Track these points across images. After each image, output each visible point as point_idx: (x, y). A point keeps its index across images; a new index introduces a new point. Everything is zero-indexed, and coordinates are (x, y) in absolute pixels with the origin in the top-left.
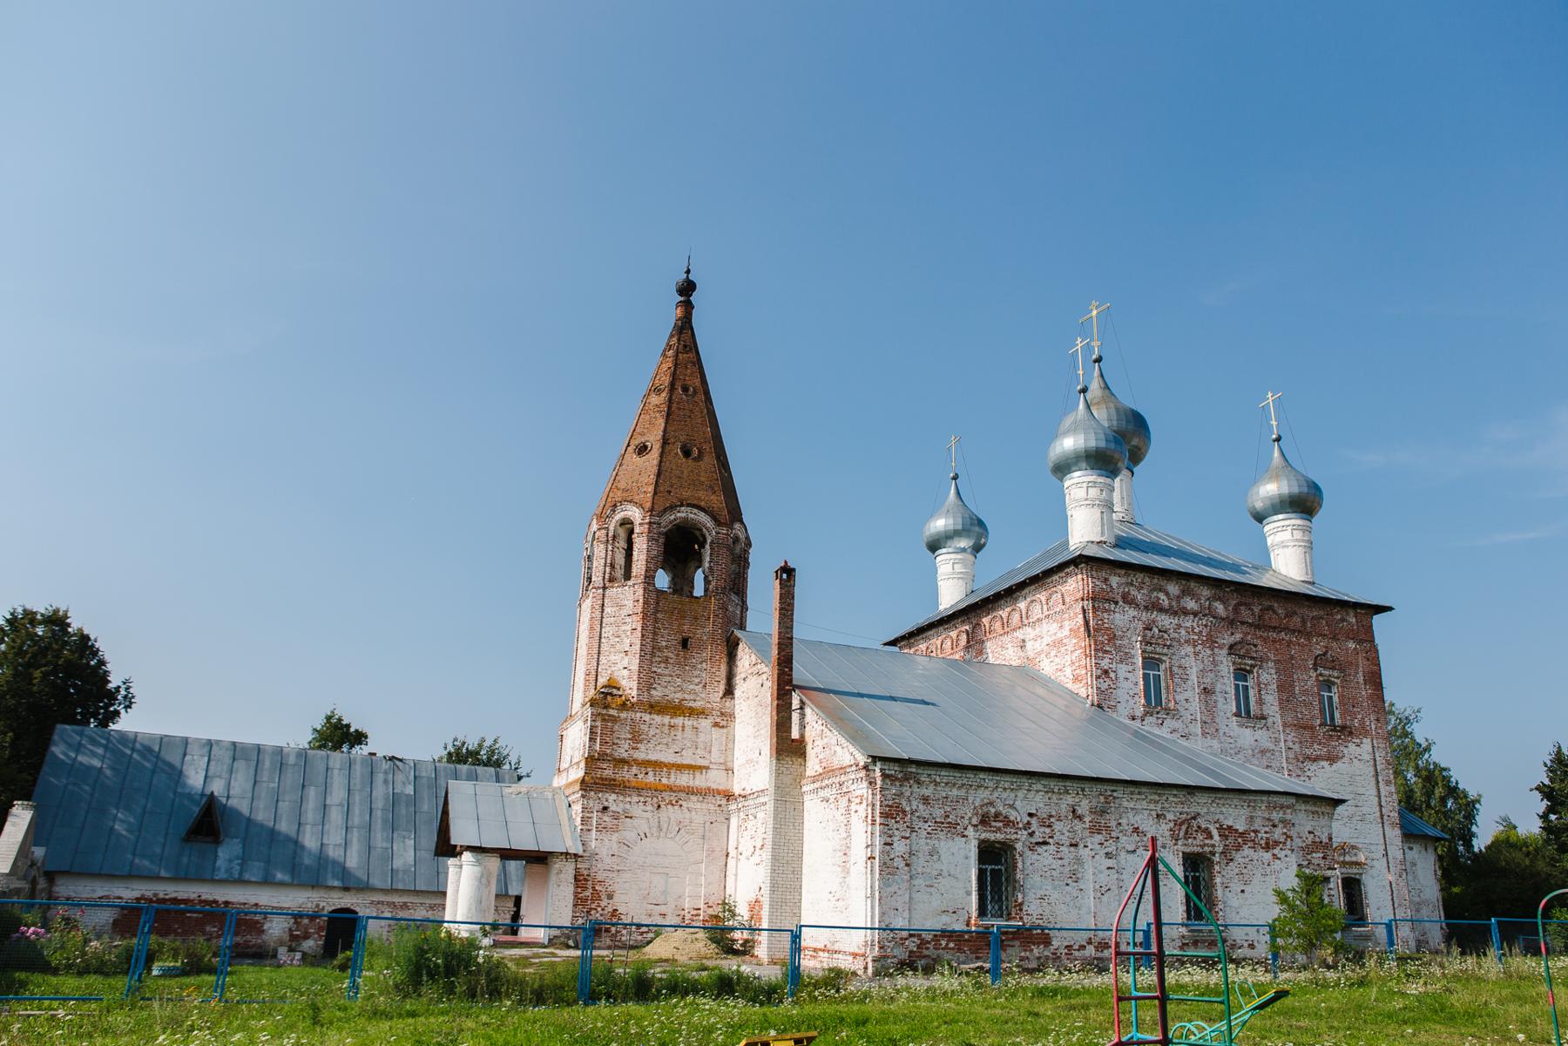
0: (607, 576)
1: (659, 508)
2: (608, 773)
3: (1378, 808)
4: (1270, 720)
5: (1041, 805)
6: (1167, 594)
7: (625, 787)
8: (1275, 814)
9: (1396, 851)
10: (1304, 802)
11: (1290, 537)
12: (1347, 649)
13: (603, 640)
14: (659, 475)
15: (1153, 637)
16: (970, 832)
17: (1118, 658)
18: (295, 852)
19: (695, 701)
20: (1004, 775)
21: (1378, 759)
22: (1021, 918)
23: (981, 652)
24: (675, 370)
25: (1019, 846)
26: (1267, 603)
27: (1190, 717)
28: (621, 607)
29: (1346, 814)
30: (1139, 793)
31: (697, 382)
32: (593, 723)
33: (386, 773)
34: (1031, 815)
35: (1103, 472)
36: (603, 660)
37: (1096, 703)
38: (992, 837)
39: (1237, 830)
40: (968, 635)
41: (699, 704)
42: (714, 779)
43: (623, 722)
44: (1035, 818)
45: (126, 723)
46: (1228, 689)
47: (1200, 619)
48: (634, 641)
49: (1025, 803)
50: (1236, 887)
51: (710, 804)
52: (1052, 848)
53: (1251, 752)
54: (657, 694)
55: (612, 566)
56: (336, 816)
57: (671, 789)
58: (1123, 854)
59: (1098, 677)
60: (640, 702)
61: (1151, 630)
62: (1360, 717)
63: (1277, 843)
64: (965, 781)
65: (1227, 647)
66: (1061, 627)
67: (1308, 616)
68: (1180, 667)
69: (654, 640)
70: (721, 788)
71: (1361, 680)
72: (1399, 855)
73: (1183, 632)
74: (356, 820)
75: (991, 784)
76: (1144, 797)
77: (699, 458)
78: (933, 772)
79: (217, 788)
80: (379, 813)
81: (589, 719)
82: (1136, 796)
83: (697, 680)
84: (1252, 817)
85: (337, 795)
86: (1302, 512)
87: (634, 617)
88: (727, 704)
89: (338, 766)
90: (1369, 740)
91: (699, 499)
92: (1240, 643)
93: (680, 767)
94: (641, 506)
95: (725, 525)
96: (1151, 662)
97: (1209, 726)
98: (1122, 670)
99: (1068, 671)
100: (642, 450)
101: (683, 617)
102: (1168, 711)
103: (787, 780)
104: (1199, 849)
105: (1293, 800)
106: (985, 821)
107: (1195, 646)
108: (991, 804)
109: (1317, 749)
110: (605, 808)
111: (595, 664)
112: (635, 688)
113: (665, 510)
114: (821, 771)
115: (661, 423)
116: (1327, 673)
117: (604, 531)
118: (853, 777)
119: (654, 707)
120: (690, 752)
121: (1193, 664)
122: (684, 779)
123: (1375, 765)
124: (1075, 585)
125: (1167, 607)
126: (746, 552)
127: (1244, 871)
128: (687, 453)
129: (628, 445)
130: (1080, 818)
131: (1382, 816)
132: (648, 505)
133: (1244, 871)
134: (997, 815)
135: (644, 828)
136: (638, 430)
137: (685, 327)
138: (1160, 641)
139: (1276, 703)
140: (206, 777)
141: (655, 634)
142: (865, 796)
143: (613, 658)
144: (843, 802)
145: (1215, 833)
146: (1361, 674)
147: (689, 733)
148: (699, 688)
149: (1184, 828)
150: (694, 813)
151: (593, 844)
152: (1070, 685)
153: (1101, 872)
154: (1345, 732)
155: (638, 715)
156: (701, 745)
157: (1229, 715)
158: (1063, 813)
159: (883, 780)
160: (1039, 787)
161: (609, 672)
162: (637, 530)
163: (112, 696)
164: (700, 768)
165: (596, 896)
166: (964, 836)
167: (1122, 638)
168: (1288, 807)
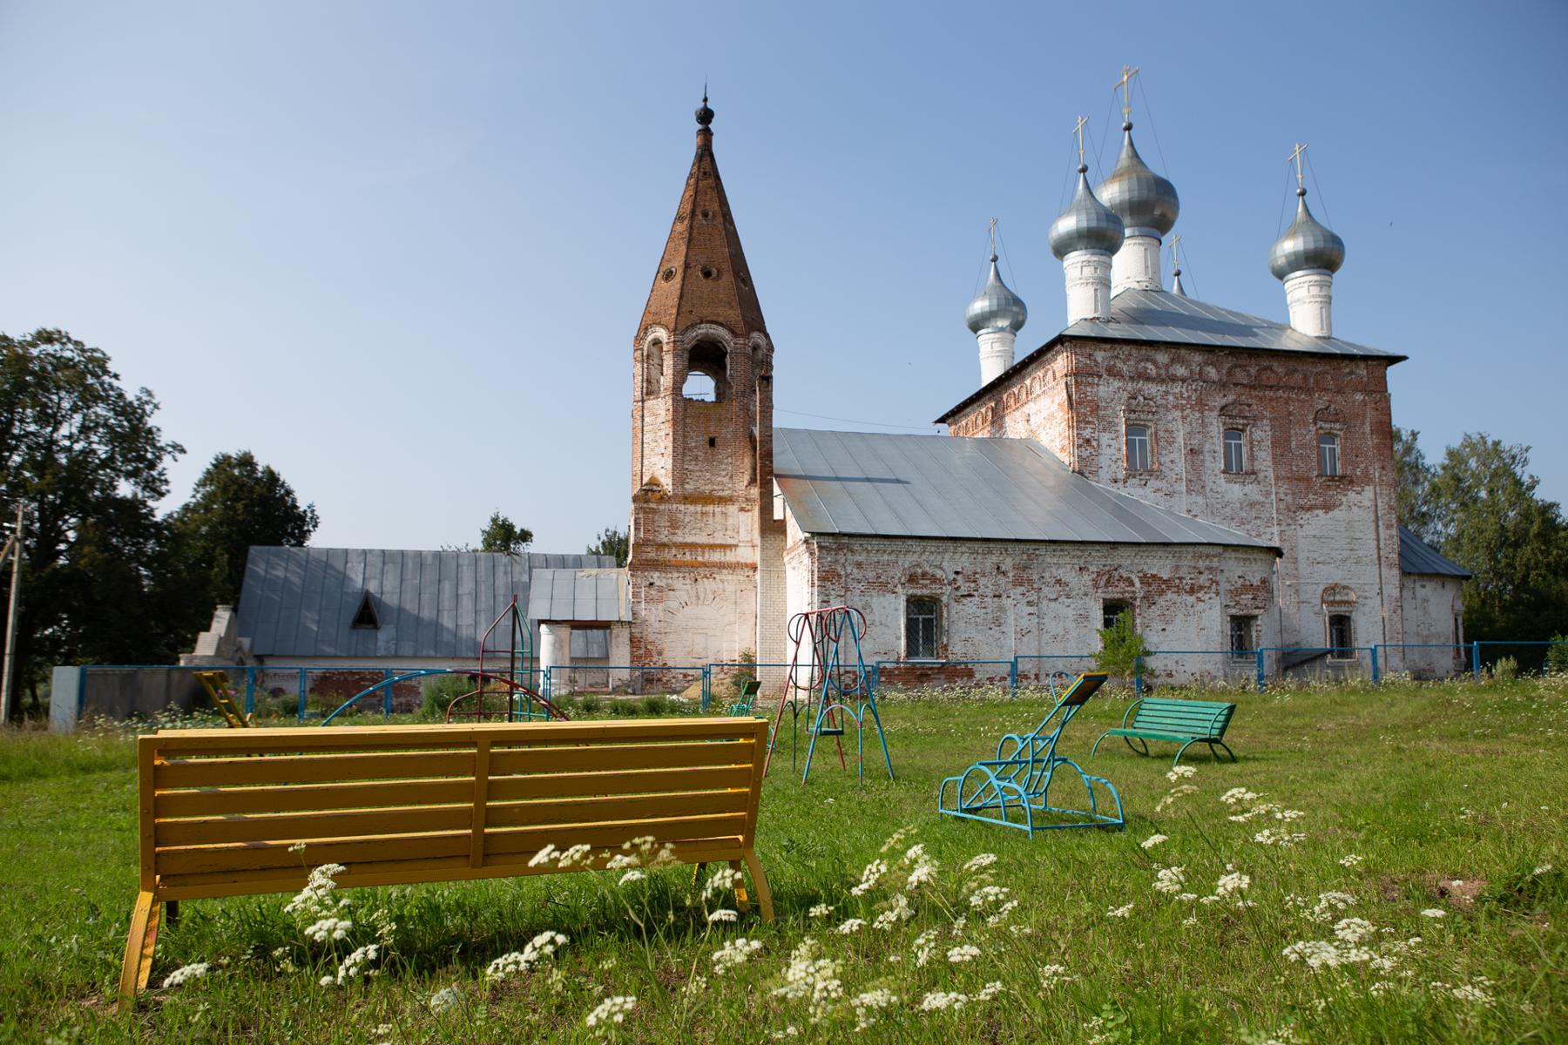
0: (645, 390)
1: (681, 327)
2: (652, 555)
3: (1376, 551)
4: (1261, 475)
5: (967, 564)
6: (1155, 363)
7: (666, 566)
8: (1201, 562)
9: (1392, 590)
10: (1234, 550)
11: (1307, 294)
12: (1354, 402)
14: (681, 297)
15: (1138, 405)
16: (899, 589)
17: (1101, 427)
18: (436, 632)
21: (1379, 504)
22: (946, 657)
23: (1001, 427)
24: (695, 198)
25: (944, 599)
26: (1267, 363)
27: (1175, 477)
28: (656, 416)
29: (1340, 557)
30: (1061, 550)
31: (716, 206)
33: (505, 565)
35: (1097, 251)
37: (1077, 469)
38: (919, 592)
41: (727, 492)
43: (662, 513)
44: (960, 576)
45: (317, 540)
46: (1217, 448)
49: (950, 563)
51: (740, 576)
52: (976, 599)
53: (1238, 505)
54: (690, 487)
56: (466, 603)
57: (704, 565)
58: (1045, 602)
59: (1079, 446)
60: (675, 495)
62: (1363, 466)
63: (1201, 588)
64: (894, 548)
65: (1218, 409)
67: (1312, 372)
68: (1166, 431)
69: (684, 442)
70: (749, 561)
71: (1367, 429)
72: (1396, 592)
73: (1171, 398)
74: (483, 605)
75: (918, 549)
77: (719, 276)
79: (373, 587)
80: (502, 599)
82: (1058, 553)
83: (724, 473)
84: (1177, 566)
85: (467, 586)
86: (1319, 267)
89: (466, 562)
90: (1371, 487)
91: (718, 315)
92: (1233, 404)
93: (713, 547)
94: (666, 327)
95: (742, 336)
96: (1134, 428)
97: (1196, 484)
100: (668, 275)
101: (709, 420)
102: (1151, 473)
103: (771, 553)
104: (1120, 596)
105: (1221, 550)
106: (912, 579)
107: (1183, 410)
108: (918, 565)
109: (1312, 499)
110: (651, 584)
113: (687, 329)
115: (683, 248)
116: (1327, 426)
117: (639, 352)
119: (688, 499)
120: (721, 533)
121: (1181, 427)
122: (716, 557)
123: (1376, 511)
124: (1061, 363)
125: (1155, 376)
128: (707, 274)
129: (658, 272)
130: (1004, 573)
131: (1379, 558)
132: (672, 326)
134: (924, 575)
135: (685, 598)
136: (666, 257)
137: (705, 154)
138: (1145, 408)
139: (1270, 458)
140: (364, 579)
141: (685, 436)
143: (653, 460)
146: (1368, 424)
147: (718, 518)
148: (726, 480)
149: (1105, 578)
151: (643, 613)
153: (1022, 617)
154: (1345, 481)
155: (675, 506)
156: (729, 528)
157: (1217, 472)
158: (988, 570)
159: (819, 551)
160: (964, 549)
163: (301, 518)
165: (648, 653)
167: (1105, 408)
168: (1214, 556)
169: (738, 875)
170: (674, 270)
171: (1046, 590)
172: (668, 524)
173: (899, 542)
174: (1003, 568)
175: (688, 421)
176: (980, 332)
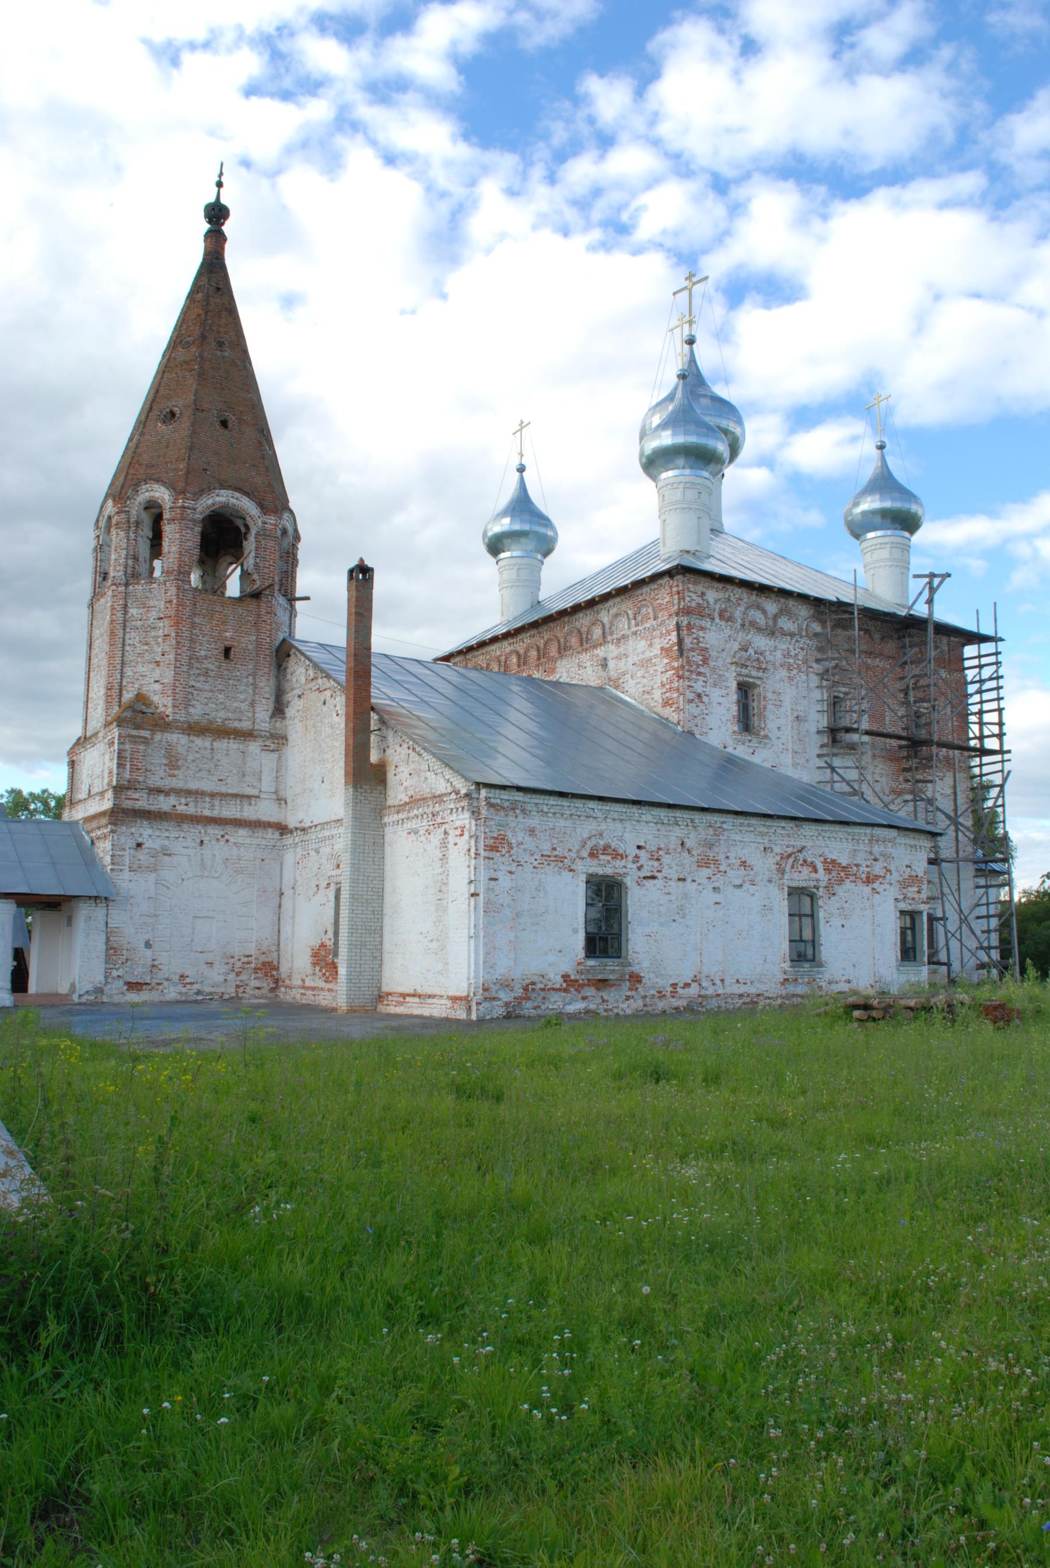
0: (129, 571)
3: (954, 844)
5: (650, 837)
6: (764, 612)
13: (127, 648)
19: (240, 720)
20: (614, 805)
25: (629, 881)
27: (782, 747)
30: (749, 825)
32: (122, 747)
34: (639, 847)
36: (128, 671)
38: (600, 871)
39: (840, 864)
40: (538, 650)
42: (265, 810)
44: (643, 851)
47: (797, 641)
48: (167, 648)
50: (836, 922)
52: (659, 883)
54: (197, 712)
55: (136, 558)
61: (746, 651)
64: (573, 811)
66: (651, 645)
76: (752, 829)
78: (541, 801)
81: (116, 741)
83: (242, 697)
87: (167, 622)
88: (278, 724)
98: (715, 694)
99: (657, 694)
101: (224, 623)
110: (139, 845)
111: (119, 677)
112: (170, 705)
114: (407, 800)
117: (123, 515)
118: (452, 806)
119: (195, 729)
122: (230, 811)
123: (955, 800)
126: (294, 547)
127: (846, 905)
133: (846, 905)
136: (162, 392)
141: (192, 641)
142: (467, 826)
143: (140, 669)
144: (438, 835)
145: (820, 867)
149: (791, 860)
150: (242, 849)
152: (659, 709)
160: (649, 818)
161: (136, 686)
162: (166, 516)
164: (249, 797)
166: (571, 870)
169: (1021, 1408)
170: (176, 409)
171: (731, 873)
172: (165, 761)
173: (579, 803)
174: (688, 844)
175: (197, 620)
176: (502, 555)
